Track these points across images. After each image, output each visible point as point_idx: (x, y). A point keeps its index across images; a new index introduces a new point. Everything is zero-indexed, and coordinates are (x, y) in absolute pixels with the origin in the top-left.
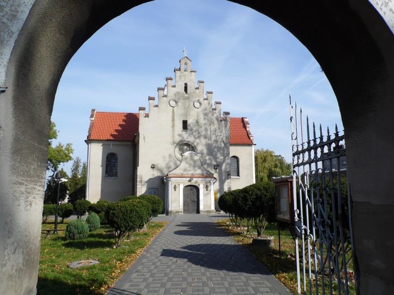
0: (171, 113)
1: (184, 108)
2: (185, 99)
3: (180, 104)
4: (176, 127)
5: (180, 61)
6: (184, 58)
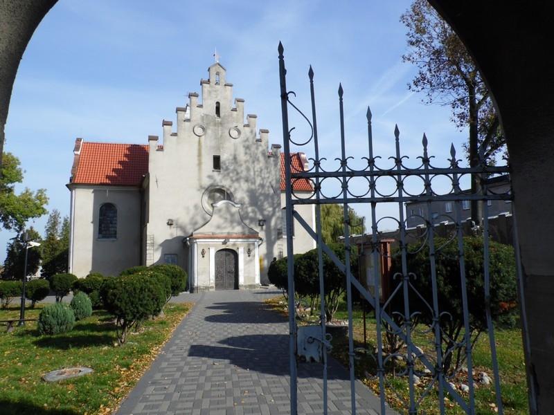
0: (196, 145)
1: (216, 138)
2: (215, 124)
3: (209, 132)
4: (203, 166)
5: (209, 70)
6: (215, 65)
